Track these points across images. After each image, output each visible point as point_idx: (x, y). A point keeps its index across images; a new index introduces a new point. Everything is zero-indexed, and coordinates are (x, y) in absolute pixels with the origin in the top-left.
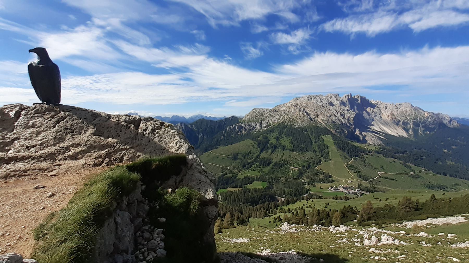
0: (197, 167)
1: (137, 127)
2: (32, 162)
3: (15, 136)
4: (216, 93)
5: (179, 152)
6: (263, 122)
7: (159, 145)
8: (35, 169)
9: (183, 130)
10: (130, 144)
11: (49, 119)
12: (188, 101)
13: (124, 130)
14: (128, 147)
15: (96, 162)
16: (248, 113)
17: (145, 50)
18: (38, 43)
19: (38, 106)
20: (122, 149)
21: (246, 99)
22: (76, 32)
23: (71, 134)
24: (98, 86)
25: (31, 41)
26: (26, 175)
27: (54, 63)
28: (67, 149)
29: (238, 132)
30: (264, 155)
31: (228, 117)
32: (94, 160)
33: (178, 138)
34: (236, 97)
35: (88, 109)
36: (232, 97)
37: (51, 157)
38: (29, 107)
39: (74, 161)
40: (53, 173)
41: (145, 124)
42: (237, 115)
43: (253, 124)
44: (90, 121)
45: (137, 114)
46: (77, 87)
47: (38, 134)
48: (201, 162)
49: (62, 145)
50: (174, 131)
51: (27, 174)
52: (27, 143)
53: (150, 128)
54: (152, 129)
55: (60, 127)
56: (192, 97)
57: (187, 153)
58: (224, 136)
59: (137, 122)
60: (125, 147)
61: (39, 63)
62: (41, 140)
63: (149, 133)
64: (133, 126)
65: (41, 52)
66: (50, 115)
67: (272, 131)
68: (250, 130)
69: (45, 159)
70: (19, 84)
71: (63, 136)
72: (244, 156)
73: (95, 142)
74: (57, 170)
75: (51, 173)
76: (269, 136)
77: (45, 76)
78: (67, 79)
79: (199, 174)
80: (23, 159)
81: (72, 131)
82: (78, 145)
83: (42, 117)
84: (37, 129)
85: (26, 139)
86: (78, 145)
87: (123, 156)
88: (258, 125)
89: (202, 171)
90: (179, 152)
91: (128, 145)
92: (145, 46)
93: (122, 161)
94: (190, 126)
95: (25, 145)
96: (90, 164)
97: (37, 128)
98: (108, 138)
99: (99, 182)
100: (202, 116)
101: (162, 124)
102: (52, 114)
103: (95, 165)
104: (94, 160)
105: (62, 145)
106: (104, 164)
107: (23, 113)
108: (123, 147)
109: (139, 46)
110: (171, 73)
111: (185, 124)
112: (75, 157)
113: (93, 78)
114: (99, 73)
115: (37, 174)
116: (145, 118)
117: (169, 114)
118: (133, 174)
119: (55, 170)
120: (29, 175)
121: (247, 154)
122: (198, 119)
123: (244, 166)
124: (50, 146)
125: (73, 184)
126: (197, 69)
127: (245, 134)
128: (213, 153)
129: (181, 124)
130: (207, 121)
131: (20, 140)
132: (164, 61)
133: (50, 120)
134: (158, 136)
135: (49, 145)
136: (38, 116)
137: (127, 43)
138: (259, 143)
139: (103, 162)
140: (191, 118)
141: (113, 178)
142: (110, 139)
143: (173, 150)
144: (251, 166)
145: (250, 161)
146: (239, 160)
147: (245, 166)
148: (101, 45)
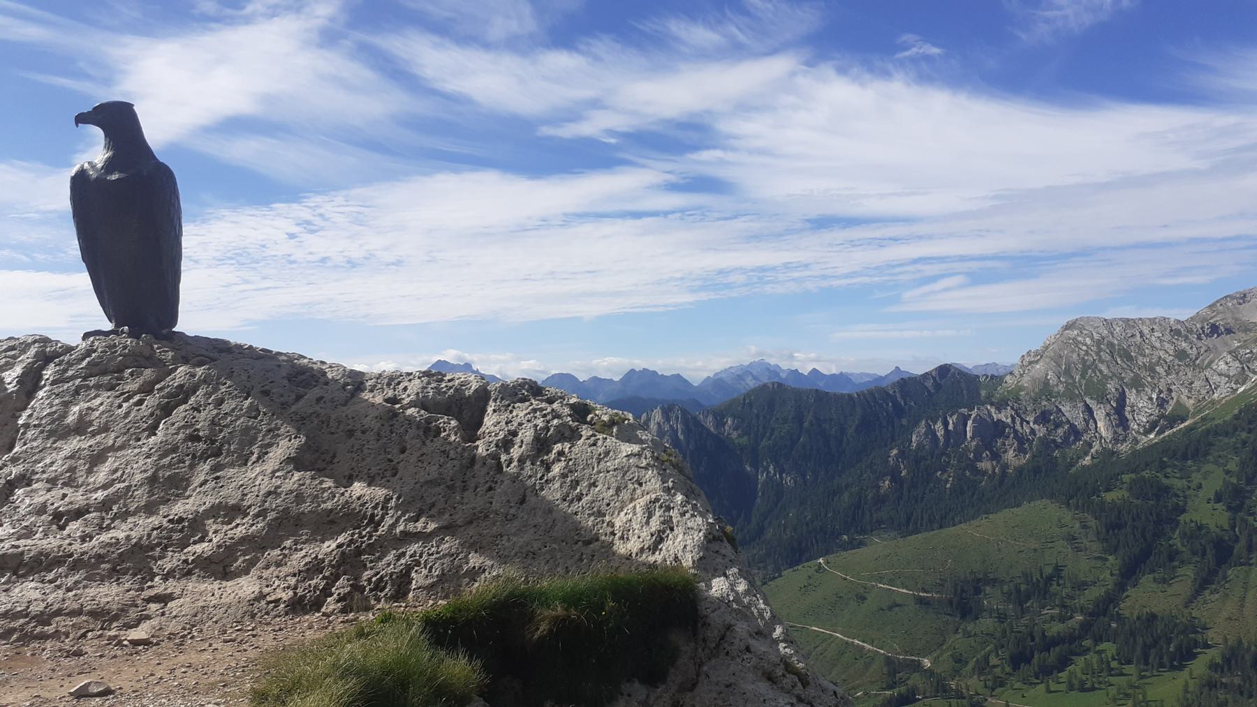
0: (753, 643)
1: (471, 428)
2: (70, 581)
3: (15, 470)
4: (853, 243)
5: (658, 557)
6: (1131, 396)
7: (566, 517)
8: (78, 612)
9: (676, 443)
10: (441, 513)
11: (137, 398)
12: (703, 296)
13: (417, 442)
14: (432, 526)
15: (300, 591)
16: (1037, 346)
17: (509, 61)
18: (107, 82)
19: (99, 344)
20: (408, 537)
21: (1024, 265)
22: (248, 20)
23: (210, 462)
24: (319, 245)
25: (88, 77)
26: (44, 637)
27: (161, 158)
28: (194, 527)
29: (978, 458)
30: (1148, 597)
31: (918, 371)
32: (293, 581)
33: (653, 483)
34: (963, 259)
35: (275, 349)
36: (942, 259)
37: (134, 561)
38: (69, 349)
39: (216, 585)
40: (139, 633)
41: (504, 416)
42: (969, 357)
43: (1072, 413)
44: (284, 406)
45: (467, 367)
46: (240, 258)
47: (97, 459)
48: (775, 620)
49: (180, 508)
50: (636, 448)
51: (49, 629)
52: (56, 499)
53: (527, 434)
54: (537, 439)
55: (172, 430)
56: (721, 272)
57: (700, 563)
58: (895, 477)
59: (464, 404)
60: (420, 525)
61: (110, 166)
62: (105, 487)
63: (521, 461)
64: (454, 423)
65: (118, 121)
66: (140, 381)
67: (1194, 447)
68: (1047, 444)
69: (114, 570)
70: (40, 257)
71: (183, 469)
72: (1019, 598)
73: (300, 498)
74: (154, 622)
75: (136, 634)
76: (1178, 484)
77: (129, 218)
78: (204, 221)
79: (763, 687)
80: (39, 565)
81: (215, 448)
82: (232, 512)
83: (112, 388)
84: (92, 442)
85: (52, 482)
86: (232, 512)
87: (409, 569)
88: (1100, 414)
89: (779, 671)
90: (658, 557)
91: (431, 517)
92: (516, 45)
93: (405, 594)
94: (709, 423)
95: (51, 509)
96: (277, 601)
97: (94, 434)
98: (349, 481)
99: (310, 689)
100: (774, 371)
101: (580, 412)
102: (148, 373)
103: (298, 606)
104: (293, 581)
105: (180, 508)
106: (331, 604)
107: (48, 373)
108: (411, 527)
109: (487, 46)
110: (643, 166)
111: (684, 412)
112: (219, 567)
113: (299, 211)
114: (325, 187)
115: (84, 636)
116: (504, 387)
117: (607, 363)
118: (449, 661)
119: (148, 617)
120: (56, 635)
121: (1039, 587)
122: (751, 383)
123: (1019, 660)
124: (134, 514)
125: (212, 686)
126: (751, 128)
127: (1020, 471)
128: (834, 570)
129: (666, 413)
130: (798, 394)
131: (35, 486)
132: (596, 104)
133: (140, 402)
134: (564, 476)
135: (132, 509)
136: (98, 387)
137: (436, 39)
138: (1114, 526)
139: (326, 592)
140: (717, 383)
141: (366, 673)
142: (358, 488)
143: (633, 546)
144: (1064, 662)
145: (1055, 629)
146: (987, 623)
147: (1028, 661)
148: (333, 62)
